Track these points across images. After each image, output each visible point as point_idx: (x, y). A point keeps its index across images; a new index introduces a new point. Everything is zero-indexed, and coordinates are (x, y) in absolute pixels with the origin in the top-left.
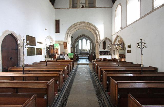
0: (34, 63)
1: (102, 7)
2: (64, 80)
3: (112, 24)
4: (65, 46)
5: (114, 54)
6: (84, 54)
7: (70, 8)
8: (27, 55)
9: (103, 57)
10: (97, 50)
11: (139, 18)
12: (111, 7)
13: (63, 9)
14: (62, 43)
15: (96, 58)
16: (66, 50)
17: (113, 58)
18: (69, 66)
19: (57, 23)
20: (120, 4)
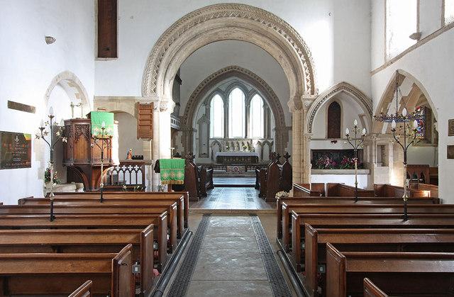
3: (370, 14)
5: (383, 163)
6: (235, 162)
10: (301, 144)
14: (130, 109)
15: (295, 182)
16: (147, 143)
17: (379, 180)
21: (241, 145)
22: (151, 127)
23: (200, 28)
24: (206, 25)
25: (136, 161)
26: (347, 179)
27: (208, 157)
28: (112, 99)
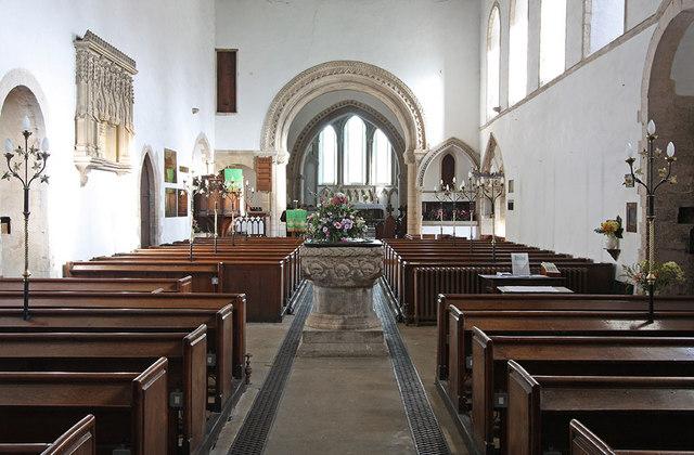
0: (68, 270)
2: (212, 400)
3: (480, 72)
4: (265, 171)
5: (492, 214)
8: (167, 216)
9: (433, 230)
11: (523, 96)
14: (250, 163)
16: (265, 196)
17: (486, 231)
18: (221, 321)
19: (226, 63)
21: (360, 193)
22: (270, 180)
23: (316, 83)
24: (322, 81)
25: (256, 212)
26: (464, 231)
28: (233, 153)
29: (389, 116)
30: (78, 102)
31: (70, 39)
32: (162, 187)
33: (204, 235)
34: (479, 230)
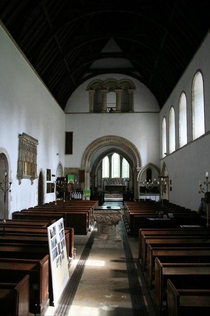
1: (144, 112)
3: (160, 140)
6: (113, 187)
7: (91, 112)
11: (203, 133)
12: (159, 112)
13: (77, 114)
19: (69, 137)
20: (200, 70)
26: (155, 198)
27: (101, 187)
29: (129, 154)
30: (19, 156)
31: (17, 135)
32: (46, 182)
33: (60, 199)
34: (160, 198)
